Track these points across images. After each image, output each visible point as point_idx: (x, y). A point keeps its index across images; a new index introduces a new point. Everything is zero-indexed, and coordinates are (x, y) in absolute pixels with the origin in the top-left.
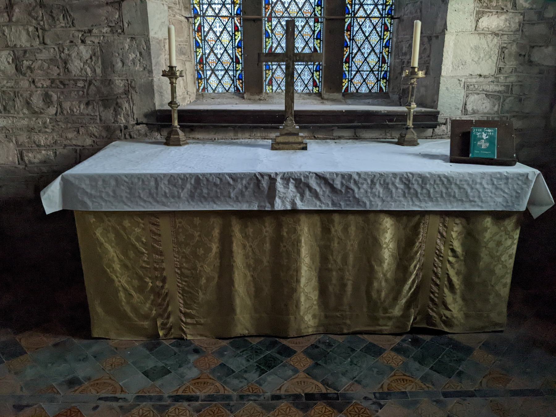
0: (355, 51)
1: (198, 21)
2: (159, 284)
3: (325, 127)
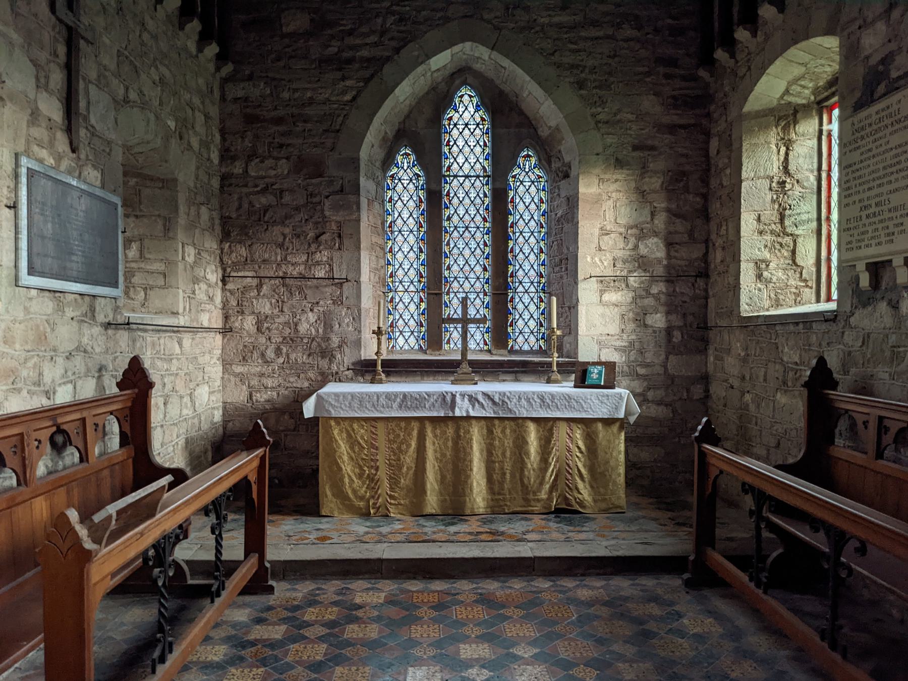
0: (517, 317)
1: (390, 295)
2: (373, 471)
3: (492, 372)
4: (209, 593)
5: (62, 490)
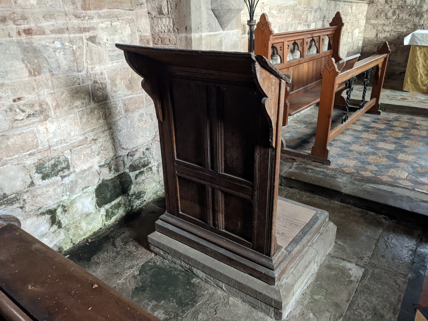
4: (354, 110)
5: (312, 61)
